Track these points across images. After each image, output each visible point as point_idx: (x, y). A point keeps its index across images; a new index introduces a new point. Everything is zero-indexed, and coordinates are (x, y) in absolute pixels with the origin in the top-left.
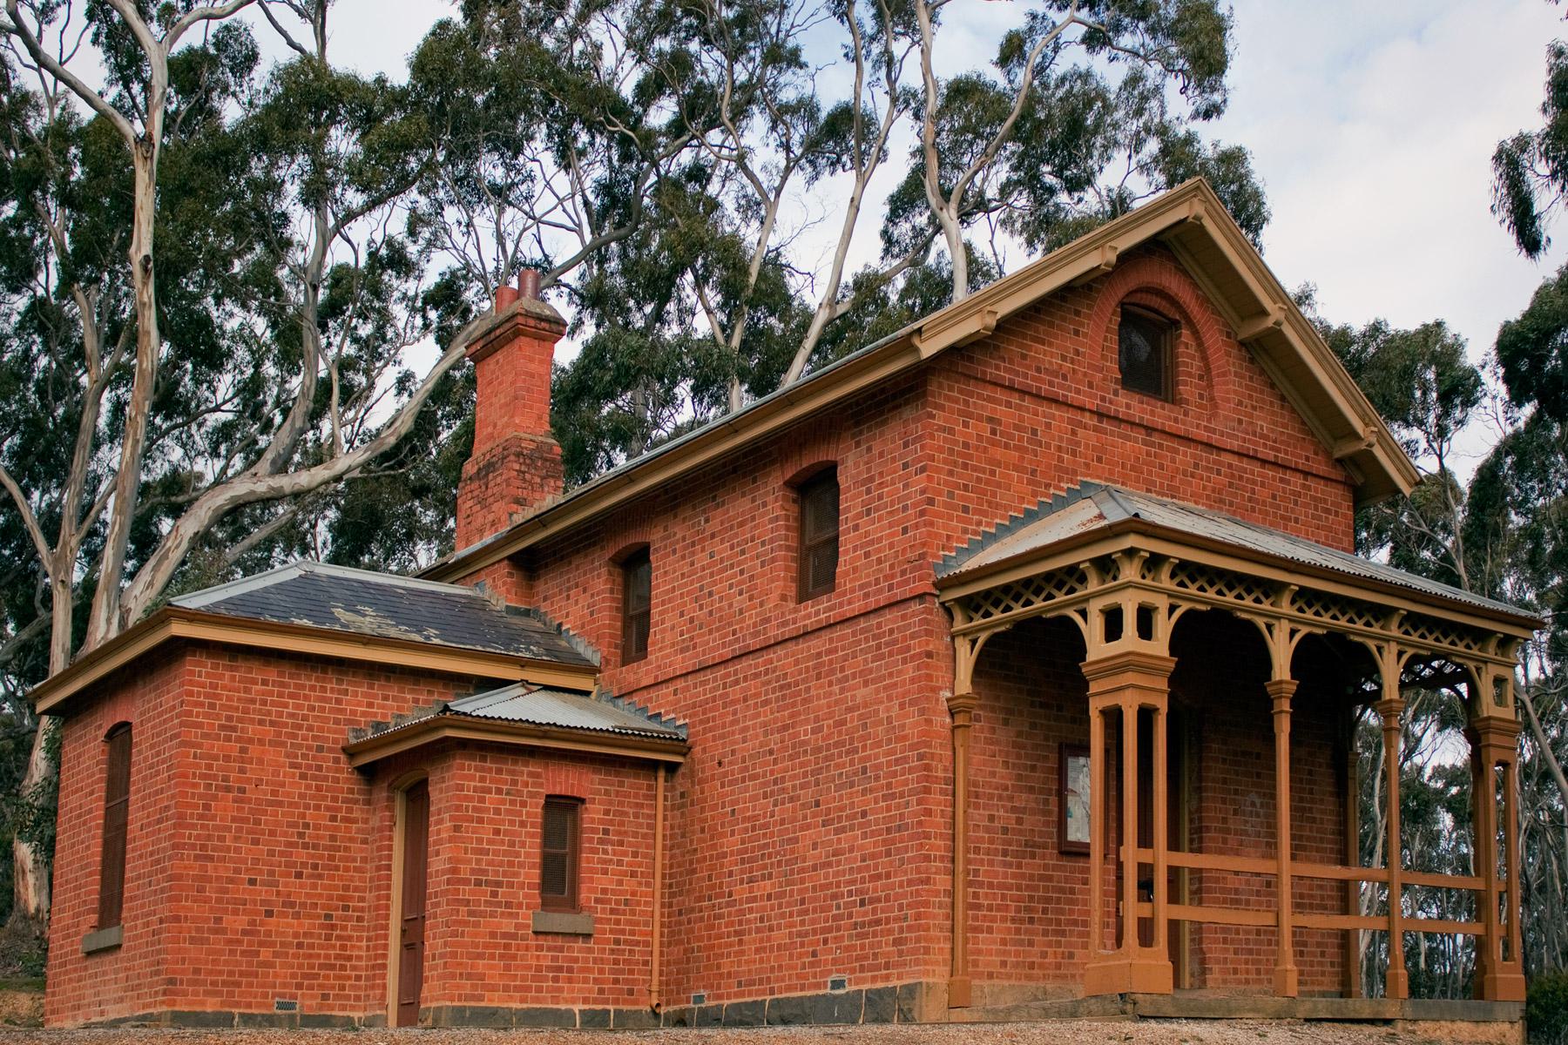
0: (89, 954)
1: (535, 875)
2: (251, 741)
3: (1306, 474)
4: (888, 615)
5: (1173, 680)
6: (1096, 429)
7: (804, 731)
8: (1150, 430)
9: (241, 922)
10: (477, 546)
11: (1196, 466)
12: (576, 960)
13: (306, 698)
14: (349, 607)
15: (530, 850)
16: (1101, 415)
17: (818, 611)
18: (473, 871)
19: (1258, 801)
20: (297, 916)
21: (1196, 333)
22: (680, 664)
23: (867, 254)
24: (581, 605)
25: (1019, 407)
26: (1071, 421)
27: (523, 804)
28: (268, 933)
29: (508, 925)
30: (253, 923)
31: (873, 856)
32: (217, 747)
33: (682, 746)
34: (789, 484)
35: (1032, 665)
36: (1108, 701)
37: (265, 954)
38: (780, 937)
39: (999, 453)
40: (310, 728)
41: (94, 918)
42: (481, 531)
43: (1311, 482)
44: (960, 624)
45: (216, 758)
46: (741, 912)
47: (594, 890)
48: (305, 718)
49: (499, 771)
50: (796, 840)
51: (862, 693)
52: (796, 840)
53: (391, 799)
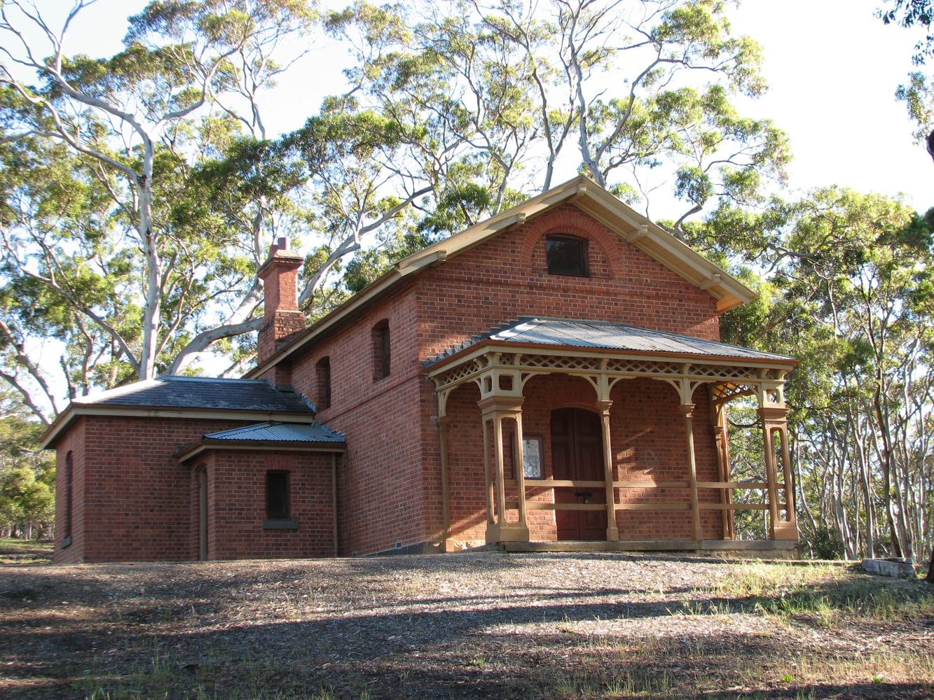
0: (64, 548)
1: (263, 505)
2: (122, 455)
6: (528, 293)
9: (122, 531)
11: (600, 303)
12: (289, 540)
13: (152, 435)
15: (259, 494)
17: (384, 384)
18: (227, 505)
19: (653, 453)
20: (152, 528)
25: (477, 289)
26: (510, 291)
27: (255, 475)
28: (137, 536)
29: (250, 527)
30: (128, 532)
31: (408, 489)
37: (135, 545)
39: (463, 310)
40: (154, 448)
45: (104, 464)
46: (366, 516)
47: (298, 510)
48: (151, 444)
49: (239, 461)
50: (382, 484)
52: (382, 484)
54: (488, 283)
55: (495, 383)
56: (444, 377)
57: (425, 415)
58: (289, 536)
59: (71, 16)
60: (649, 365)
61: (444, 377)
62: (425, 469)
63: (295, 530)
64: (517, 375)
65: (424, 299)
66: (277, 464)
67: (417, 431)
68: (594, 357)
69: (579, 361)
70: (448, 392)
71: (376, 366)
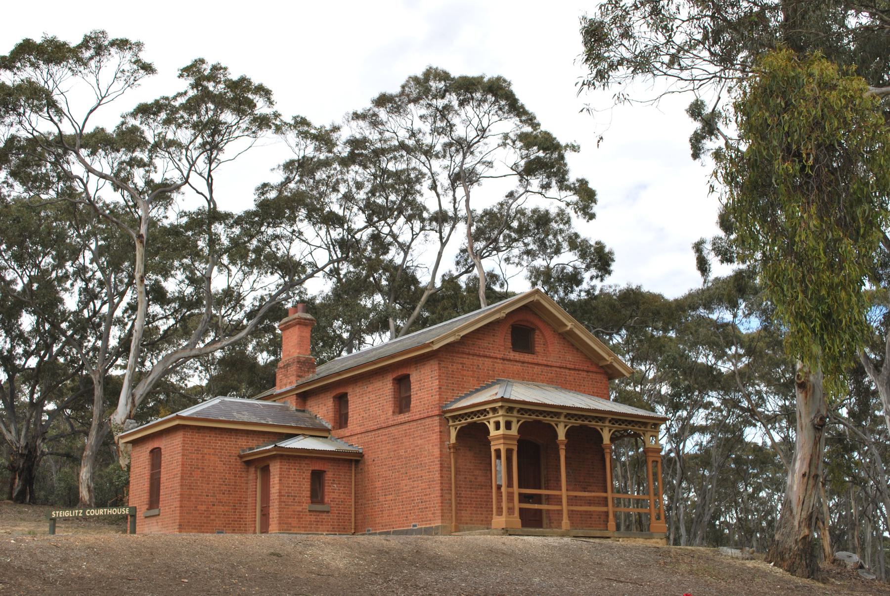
1: (308, 494)
3: (588, 372)
4: (427, 420)
5: (518, 441)
7: (402, 452)
8: (523, 362)
9: (204, 507)
10: (284, 390)
14: (238, 412)
15: (306, 486)
16: (504, 359)
21: (541, 331)
22: (359, 430)
23: (448, 266)
24: (323, 410)
29: (299, 508)
32: (194, 456)
33: (361, 455)
34: (394, 379)
35: (473, 435)
36: (497, 447)
37: (212, 517)
38: (395, 512)
39: (465, 373)
41: (147, 507)
42: (286, 385)
43: (590, 374)
44: (451, 423)
51: (420, 442)
53: (256, 471)
54: (479, 356)
55: (502, 425)
56: (455, 418)
57: (442, 442)
58: (324, 516)
59: (92, 111)
60: (541, 413)
61: (455, 418)
62: (441, 477)
63: (328, 512)
64: (514, 420)
65: (443, 364)
66: (317, 467)
67: (436, 451)
68: (556, 411)
69: (549, 413)
70: (459, 427)
71: (322, 396)
